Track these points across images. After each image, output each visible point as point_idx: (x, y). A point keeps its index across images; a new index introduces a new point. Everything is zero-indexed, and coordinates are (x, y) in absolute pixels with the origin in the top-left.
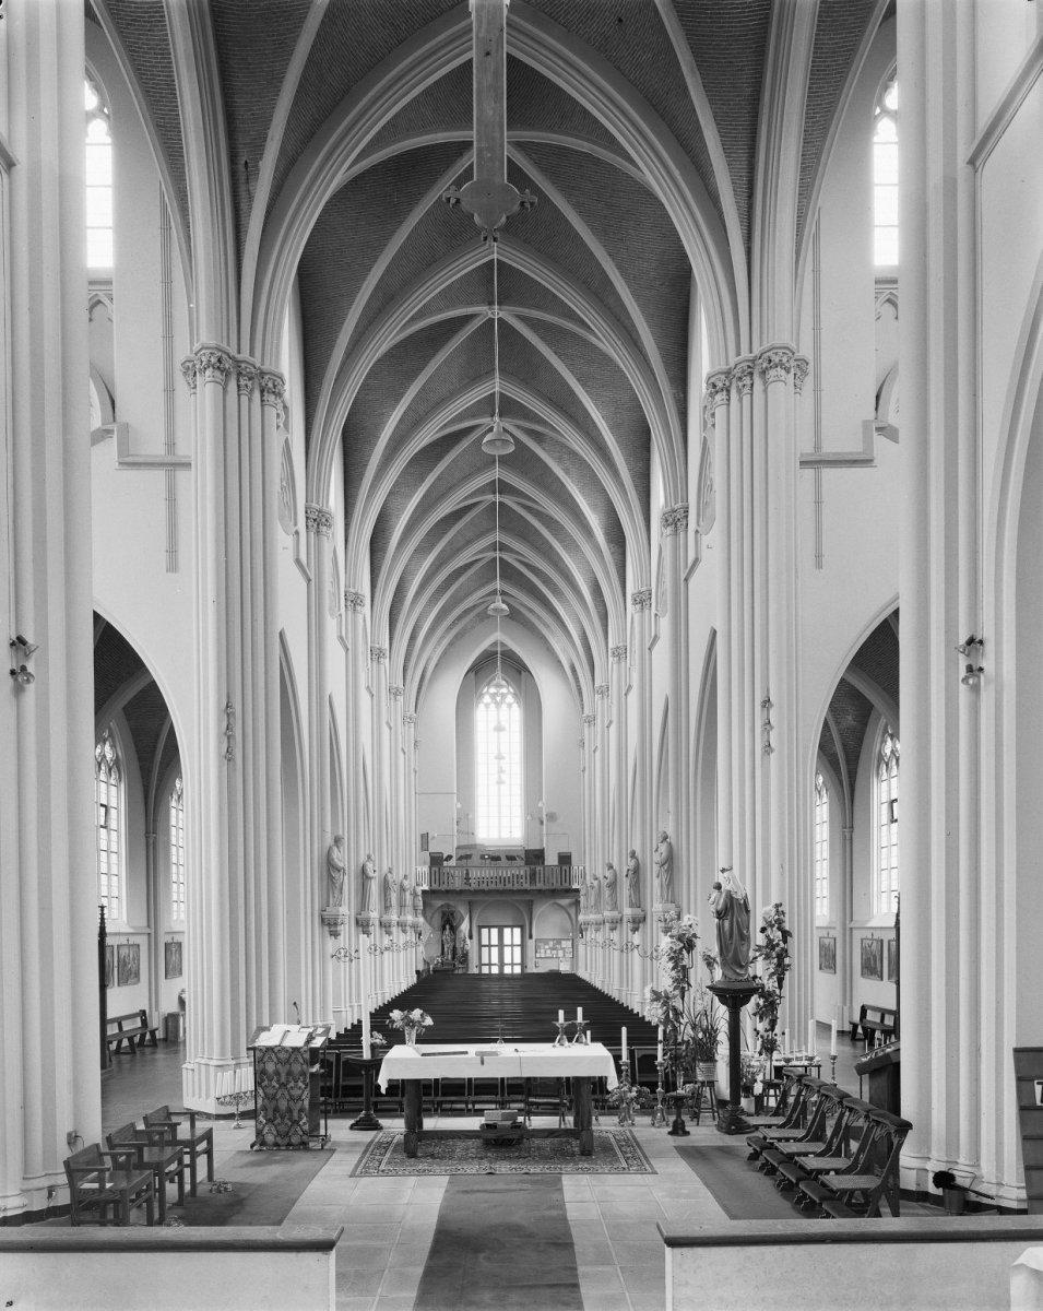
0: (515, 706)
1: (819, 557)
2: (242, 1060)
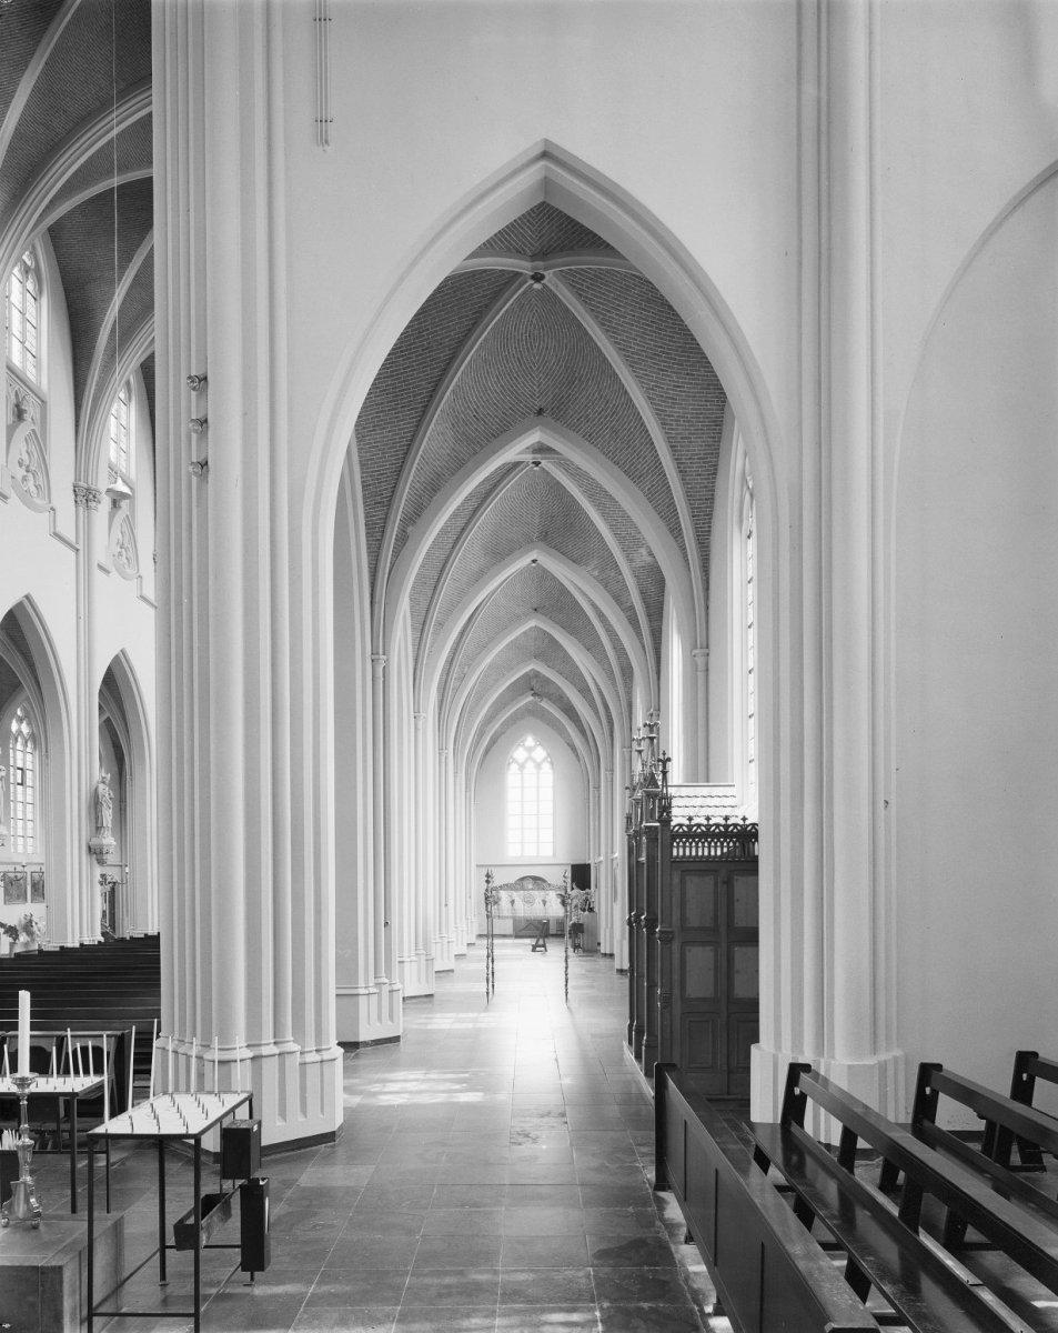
0: (546, 767)
2: (265, 1051)
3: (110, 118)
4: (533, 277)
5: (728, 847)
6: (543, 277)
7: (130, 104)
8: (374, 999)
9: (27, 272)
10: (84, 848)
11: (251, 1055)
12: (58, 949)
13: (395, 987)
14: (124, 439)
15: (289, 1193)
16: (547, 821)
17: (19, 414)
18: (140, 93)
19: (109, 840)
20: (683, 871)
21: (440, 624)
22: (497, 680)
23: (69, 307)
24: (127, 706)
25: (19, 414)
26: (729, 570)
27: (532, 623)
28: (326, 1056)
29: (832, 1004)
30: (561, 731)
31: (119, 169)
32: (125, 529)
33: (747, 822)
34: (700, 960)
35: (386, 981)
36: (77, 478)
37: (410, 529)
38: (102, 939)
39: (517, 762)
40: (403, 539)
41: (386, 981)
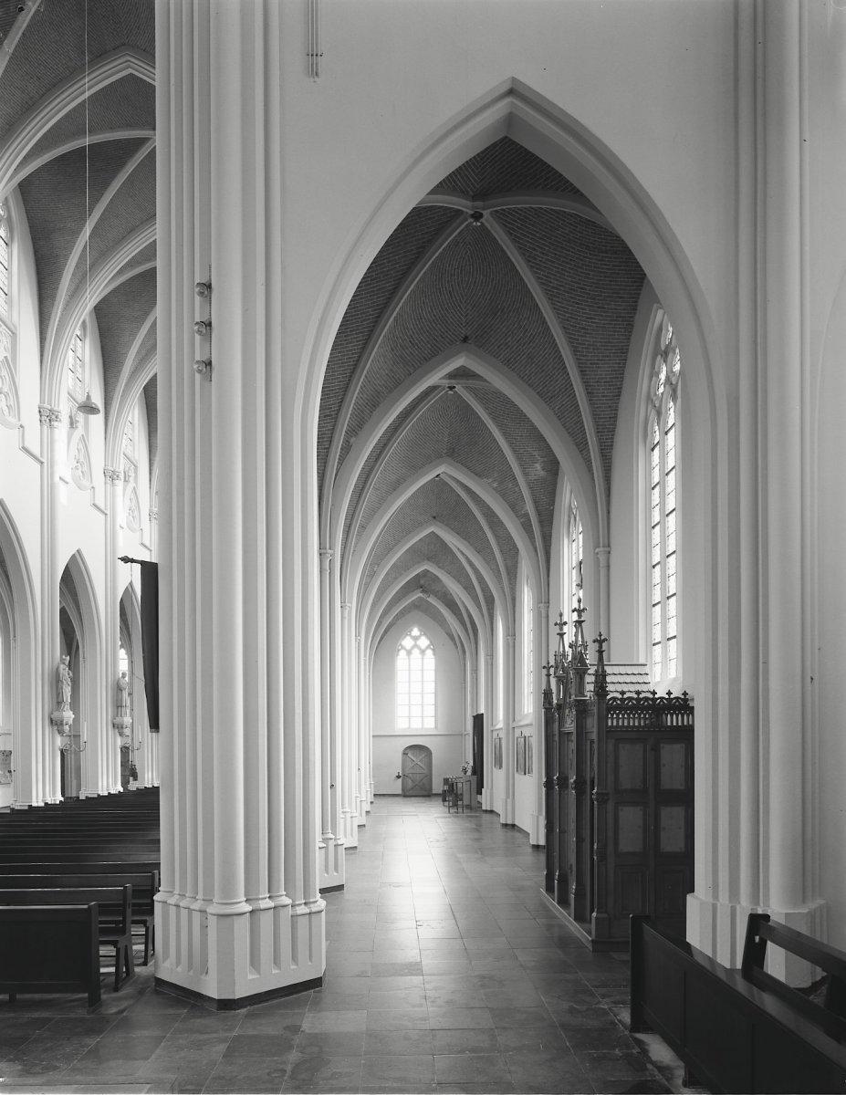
0: (429, 653)
1: (313, 55)
3: (83, 82)
4: (472, 216)
5: (645, 719)
6: (481, 216)
7: (112, 66)
10: (47, 722)
11: (250, 908)
12: (26, 808)
13: (340, 842)
14: (80, 370)
15: (297, 1040)
16: (430, 699)
18: (16, 139)
19: (68, 715)
20: (617, 740)
21: (363, 527)
22: (396, 578)
23: (36, 252)
24: (82, 602)
26: (635, 474)
27: (432, 529)
28: (314, 908)
29: (767, 859)
30: (442, 622)
31: (89, 132)
32: (81, 446)
33: (672, 696)
34: (631, 818)
35: (333, 836)
36: (42, 401)
37: (352, 440)
38: (62, 799)
39: (405, 649)
40: (347, 448)
41: (333, 836)
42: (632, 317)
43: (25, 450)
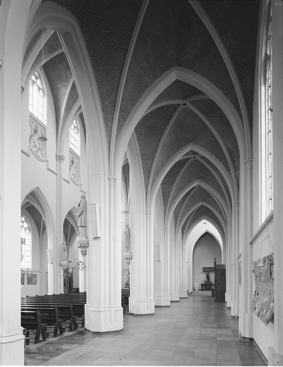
8: (146, 303)
9: (75, 128)
17: (73, 162)
21: (170, 207)
25: (73, 162)
27: (195, 184)
36: (57, 153)
42: (235, 106)
43: (49, 169)
